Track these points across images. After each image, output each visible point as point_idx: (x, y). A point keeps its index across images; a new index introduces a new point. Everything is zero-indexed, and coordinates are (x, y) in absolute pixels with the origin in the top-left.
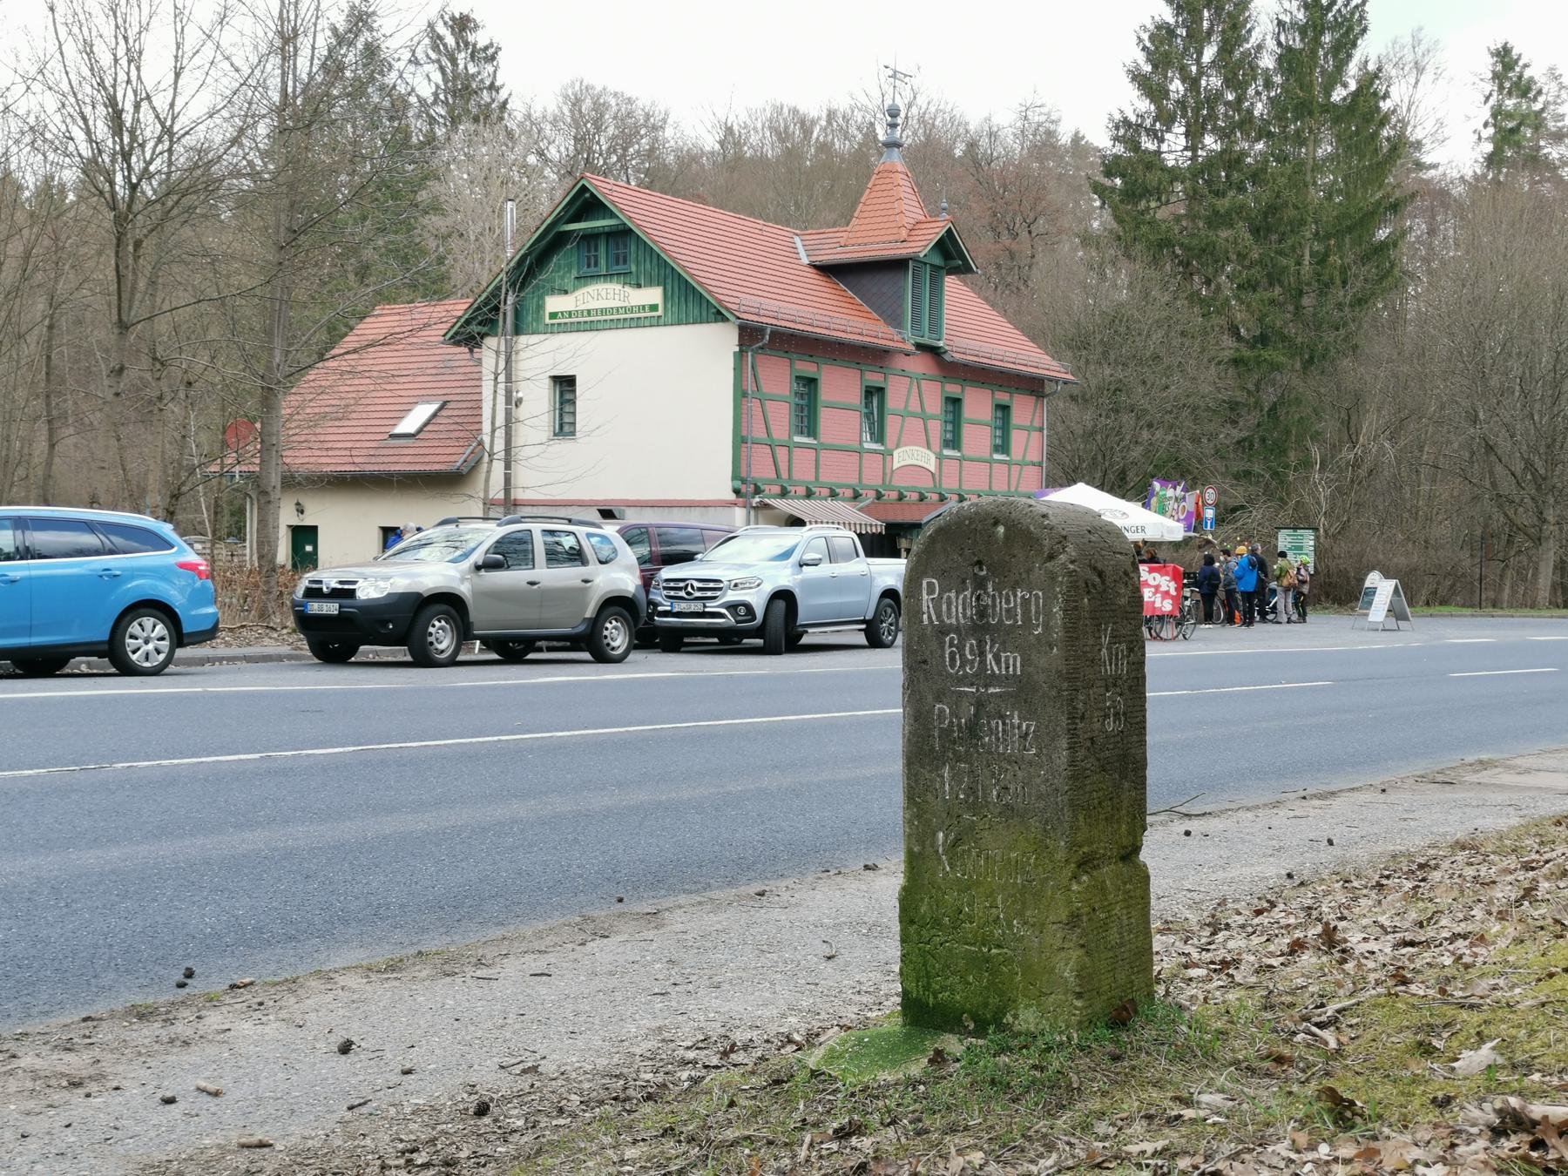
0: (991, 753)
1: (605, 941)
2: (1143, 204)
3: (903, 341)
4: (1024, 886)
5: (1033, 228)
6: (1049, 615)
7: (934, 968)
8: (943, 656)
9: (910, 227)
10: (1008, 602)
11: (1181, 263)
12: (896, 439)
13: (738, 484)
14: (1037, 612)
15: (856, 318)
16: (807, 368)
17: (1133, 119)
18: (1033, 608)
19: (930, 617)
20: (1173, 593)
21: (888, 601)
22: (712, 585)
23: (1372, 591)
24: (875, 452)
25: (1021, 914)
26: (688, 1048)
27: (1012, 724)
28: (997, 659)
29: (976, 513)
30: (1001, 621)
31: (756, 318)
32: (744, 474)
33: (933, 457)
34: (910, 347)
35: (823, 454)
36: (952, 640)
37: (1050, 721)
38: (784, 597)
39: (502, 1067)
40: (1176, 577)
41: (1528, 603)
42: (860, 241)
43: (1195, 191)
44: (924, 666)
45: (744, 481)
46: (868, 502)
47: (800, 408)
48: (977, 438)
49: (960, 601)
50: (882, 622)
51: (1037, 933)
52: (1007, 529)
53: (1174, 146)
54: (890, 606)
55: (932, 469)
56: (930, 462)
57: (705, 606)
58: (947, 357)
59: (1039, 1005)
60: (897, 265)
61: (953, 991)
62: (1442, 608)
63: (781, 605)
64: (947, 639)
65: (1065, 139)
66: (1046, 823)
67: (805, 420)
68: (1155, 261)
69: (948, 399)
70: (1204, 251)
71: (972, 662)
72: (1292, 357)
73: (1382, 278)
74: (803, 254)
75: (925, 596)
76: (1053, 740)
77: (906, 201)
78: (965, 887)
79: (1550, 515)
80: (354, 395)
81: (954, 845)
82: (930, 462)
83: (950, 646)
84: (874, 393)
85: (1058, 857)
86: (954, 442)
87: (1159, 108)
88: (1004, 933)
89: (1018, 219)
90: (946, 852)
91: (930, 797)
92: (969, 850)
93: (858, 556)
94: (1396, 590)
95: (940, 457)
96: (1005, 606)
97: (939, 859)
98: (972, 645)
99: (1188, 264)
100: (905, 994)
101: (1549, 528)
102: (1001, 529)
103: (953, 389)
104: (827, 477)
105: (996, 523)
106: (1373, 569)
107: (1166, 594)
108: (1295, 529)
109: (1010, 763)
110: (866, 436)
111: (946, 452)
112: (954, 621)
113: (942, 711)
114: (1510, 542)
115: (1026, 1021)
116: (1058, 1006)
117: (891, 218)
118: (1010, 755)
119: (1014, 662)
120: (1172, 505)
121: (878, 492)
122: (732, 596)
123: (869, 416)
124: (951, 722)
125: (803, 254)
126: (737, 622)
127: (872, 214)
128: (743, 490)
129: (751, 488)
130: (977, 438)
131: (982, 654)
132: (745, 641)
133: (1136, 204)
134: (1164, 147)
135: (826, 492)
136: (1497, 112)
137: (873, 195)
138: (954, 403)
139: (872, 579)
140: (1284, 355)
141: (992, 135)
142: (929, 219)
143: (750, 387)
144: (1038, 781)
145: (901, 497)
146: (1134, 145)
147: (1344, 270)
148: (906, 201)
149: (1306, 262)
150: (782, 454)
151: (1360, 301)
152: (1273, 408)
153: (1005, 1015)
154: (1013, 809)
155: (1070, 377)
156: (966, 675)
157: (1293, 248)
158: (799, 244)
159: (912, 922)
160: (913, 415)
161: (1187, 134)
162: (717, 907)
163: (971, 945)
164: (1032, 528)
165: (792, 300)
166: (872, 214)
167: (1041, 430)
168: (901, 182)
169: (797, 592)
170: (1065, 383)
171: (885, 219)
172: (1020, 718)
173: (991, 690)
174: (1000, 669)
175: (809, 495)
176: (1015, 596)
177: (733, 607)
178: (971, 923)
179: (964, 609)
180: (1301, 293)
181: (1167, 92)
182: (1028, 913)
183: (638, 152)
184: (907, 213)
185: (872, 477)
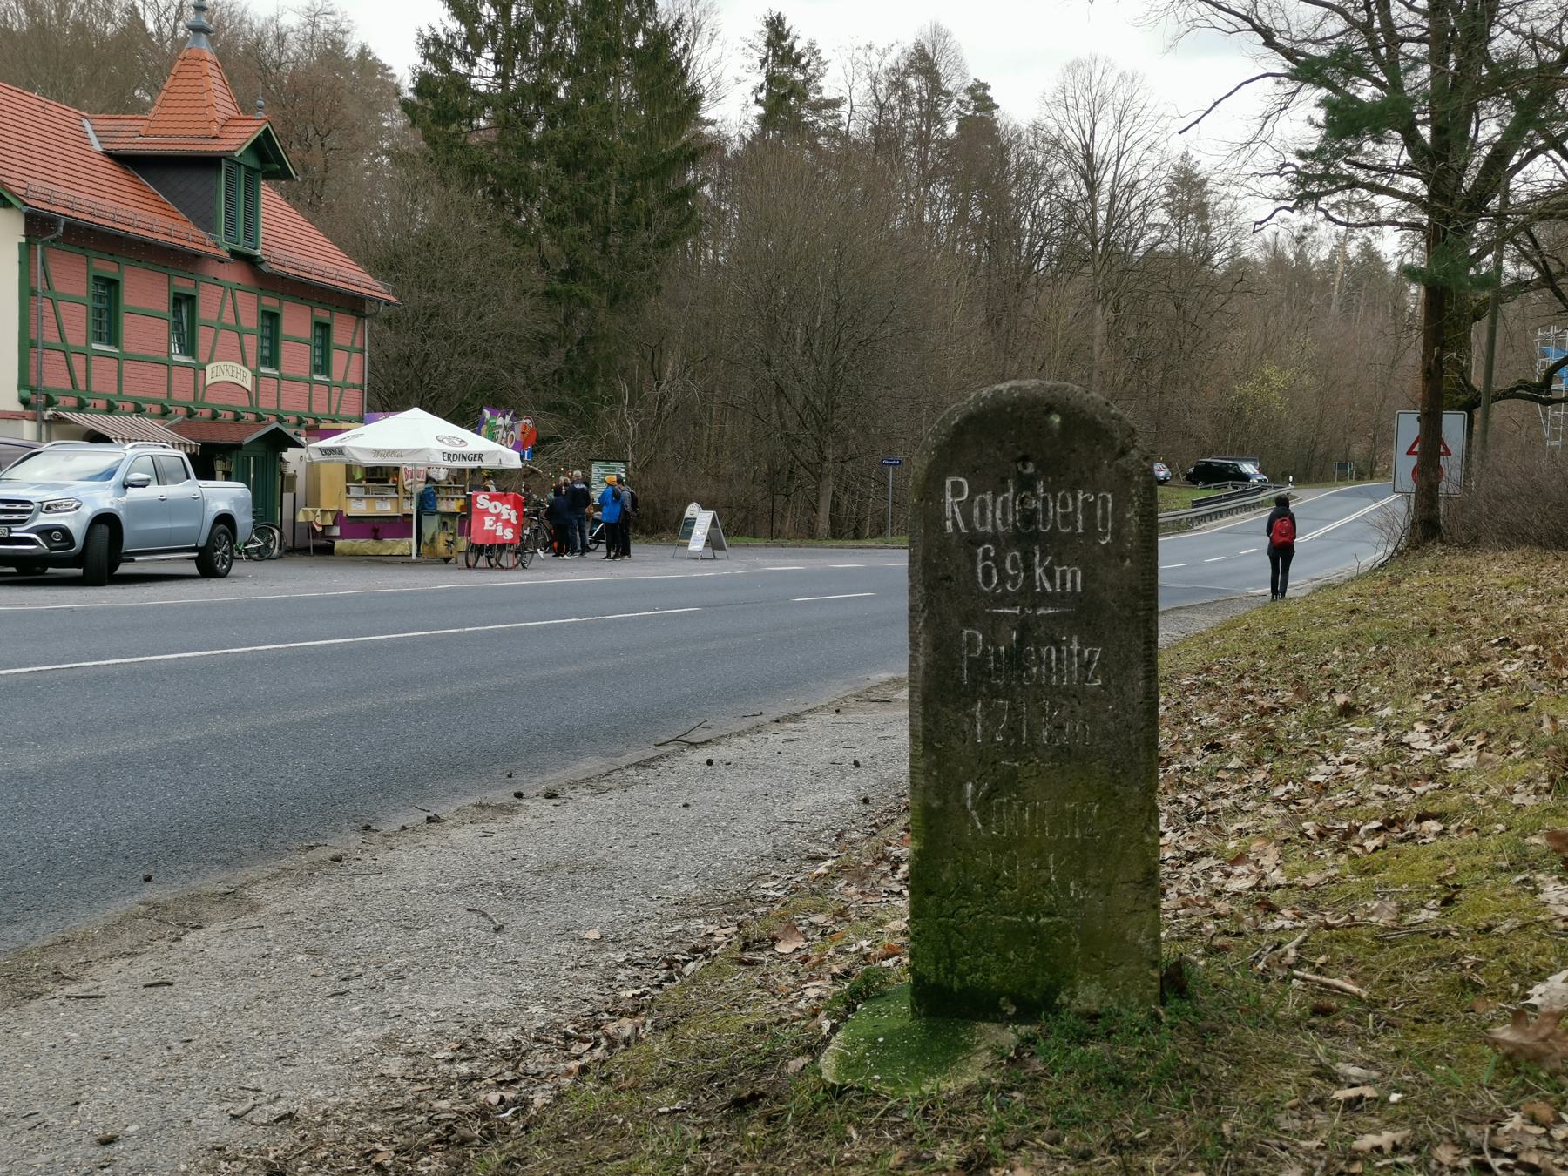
0: (1041, 686)
1: (202, 932)
2: (454, 126)
3: (217, 246)
4: (1084, 841)
5: (327, 141)
6: (1120, 522)
7: (960, 945)
8: (974, 571)
9: (222, 122)
10: (1064, 505)
11: (492, 192)
12: (208, 352)
13: (26, 394)
14: (1104, 518)
15: (162, 218)
16: (108, 269)
17: (444, 38)
18: (1099, 513)
19: (955, 524)
20: (514, 521)
21: (222, 527)
22: (18, 507)
23: (692, 522)
24: (185, 365)
25: (1080, 874)
27: (1070, 653)
28: (1050, 574)
29: (1021, 398)
30: (1054, 527)
31: (46, 206)
32: (33, 383)
33: (249, 374)
34: (223, 253)
35: (125, 364)
36: (987, 551)
37: (1121, 647)
38: (106, 522)
39: (234, 1117)
40: (517, 506)
41: (808, 533)
42: (163, 132)
43: (507, 121)
44: (947, 584)
45: (33, 391)
46: (178, 419)
47: (100, 312)
48: (296, 357)
49: (999, 505)
50: (215, 550)
51: (1102, 896)
52: (1065, 418)
53: (483, 72)
54: (224, 532)
55: (249, 387)
56: (246, 379)
57: (10, 531)
58: (264, 268)
59: (1104, 979)
60: (208, 163)
61: (987, 971)
62: (739, 539)
63: (104, 530)
64: (980, 550)
65: (352, 52)
66: (1115, 766)
67: (105, 326)
68: (468, 188)
69: (264, 312)
70: (516, 180)
71: (1014, 579)
72: (599, 293)
73: (681, 226)
74: (94, 140)
75: (949, 499)
76: (1125, 668)
77: (217, 93)
78: (1001, 847)
79: (830, 454)
81: (988, 797)
82: (246, 379)
84: (184, 301)
85: (1130, 805)
86: (271, 359)
87: (471, 31)
88: (1057, 898)
89: (311, 132)
90: (976, 806)
91: (954, 741)
92: (1009, 802)
93: (188, 478)
94: (714, 522)
95: (257, 376)
96: (1059, 510)
97: (967, 815)
98: (1014, 558)
99: (501, 193)
100: (919, 980)
101: (828, 466)
102: (1056, 419)
103: (271, 303)
104: (133, 389)
105: (1050, 409)
106: (690, 502)
107: (507, 523)
108: (608, 461)
109: (1066, 697)
110: (175, 348)
111: (263, 370)
112: (989, 528)
113: (972, 638)
114: (791, 477)
115: (1087, 1000)
116: (1130, 979)
117: (201, 111)
118: (1067, 688)
119: (1073, 578)
120: (501, 433)
121: (189, 409)
122: (44, 520)
123: (177, 326)
124: (985, 651)
125: (94, 140)
126: (52, 549)
127: (177, 103)
128: (33, 401)
129: (42, 400)
130: (296, 357)
131: (1029, 568)
132: (50, 570)
133: (447, 126)
134: (476, 71)
135: (129, 407)
136: (771, 78)
137: (178, 82)
138: (271, 318)
139: (204, 503)
140: (593, 291)
141: (280, 38)
142: (242, 116)
143: (40, 285)
144: (1104, 717)
145: (215, 416)
146: (446, 67)
147: (649, 212)
148: (217, 93)
149: (612, 202)
150: (78, 363)
151: (663, 244)
152: (581, 343)
153: (1057, 994)
154: (1069, 751)
155: (392, 298)
156: (1006, 593)
157: (602, 187)
158: (89, 128)
159: (929, 892)
160: (228, 328)
161: (497, 61)
162: (304, 878)
163: (1011, 914)
164: (1099, 418)
165: (102, 194)
166: (177, 103)
167: (362, 351)
168: (211, 72)
169: (121, 514)
170: (387, 304)
171: (194, 111)
172: (1080, 644)
173: (1041, 611)
174: (1053, 586)
175: (111, 409)
176: (1075, 499)
177: (46, 532)
178: (1012, 888)
179: (1004, 514)
180: (608, 231)
181: (479, 15)
182: (1090, 873)
184: (218, 107)
185: (183, 391)
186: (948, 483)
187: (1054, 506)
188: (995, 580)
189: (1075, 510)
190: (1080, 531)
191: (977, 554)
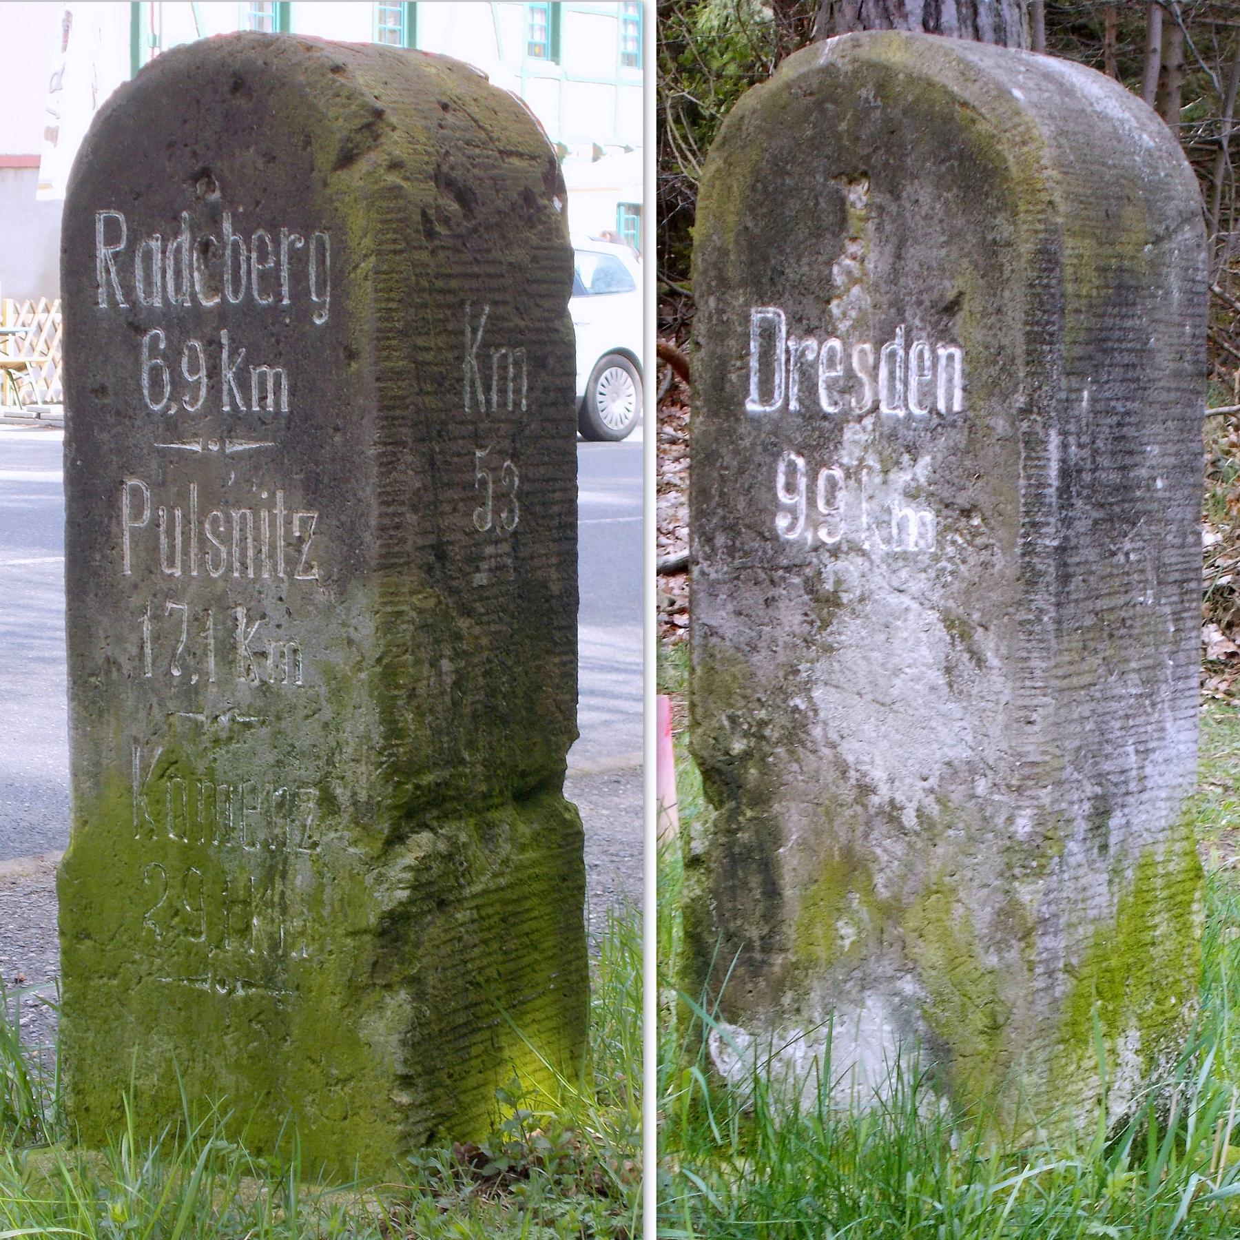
19: (111, 296)
26: (283, 893)
80: (236, 534)
83: (152, 356)
174: (248, 403)
189: (278, 263)
190: (286, 302)
191: (140, 345)
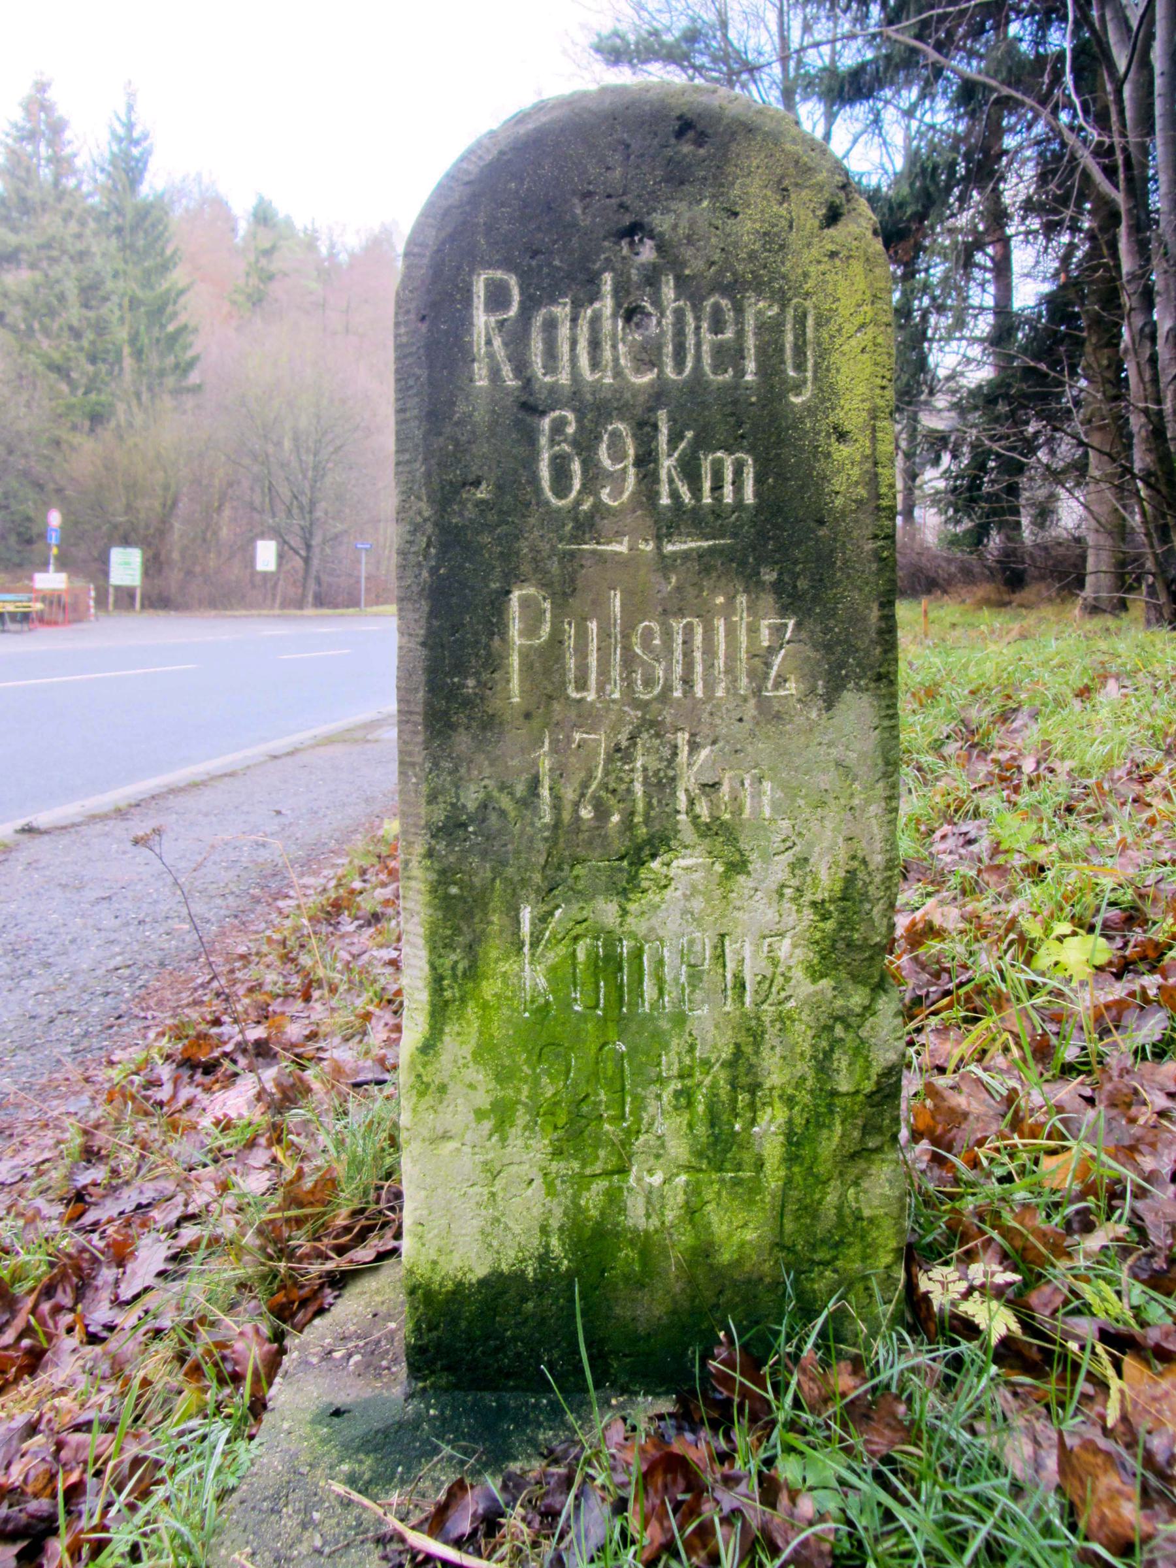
18: (789, 338)
28: (690, 471)
36: (558, 427)
174: (696, 491)
183: (25, 320)
186: (479, 289)
187: (698, 328)
188: (577, 484)
189: (740, 334)
